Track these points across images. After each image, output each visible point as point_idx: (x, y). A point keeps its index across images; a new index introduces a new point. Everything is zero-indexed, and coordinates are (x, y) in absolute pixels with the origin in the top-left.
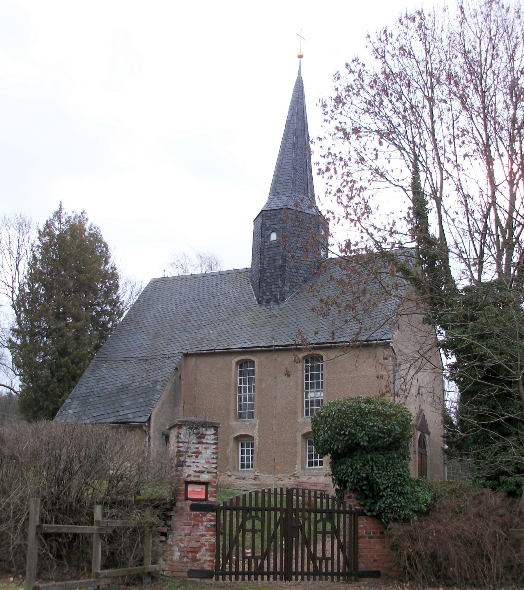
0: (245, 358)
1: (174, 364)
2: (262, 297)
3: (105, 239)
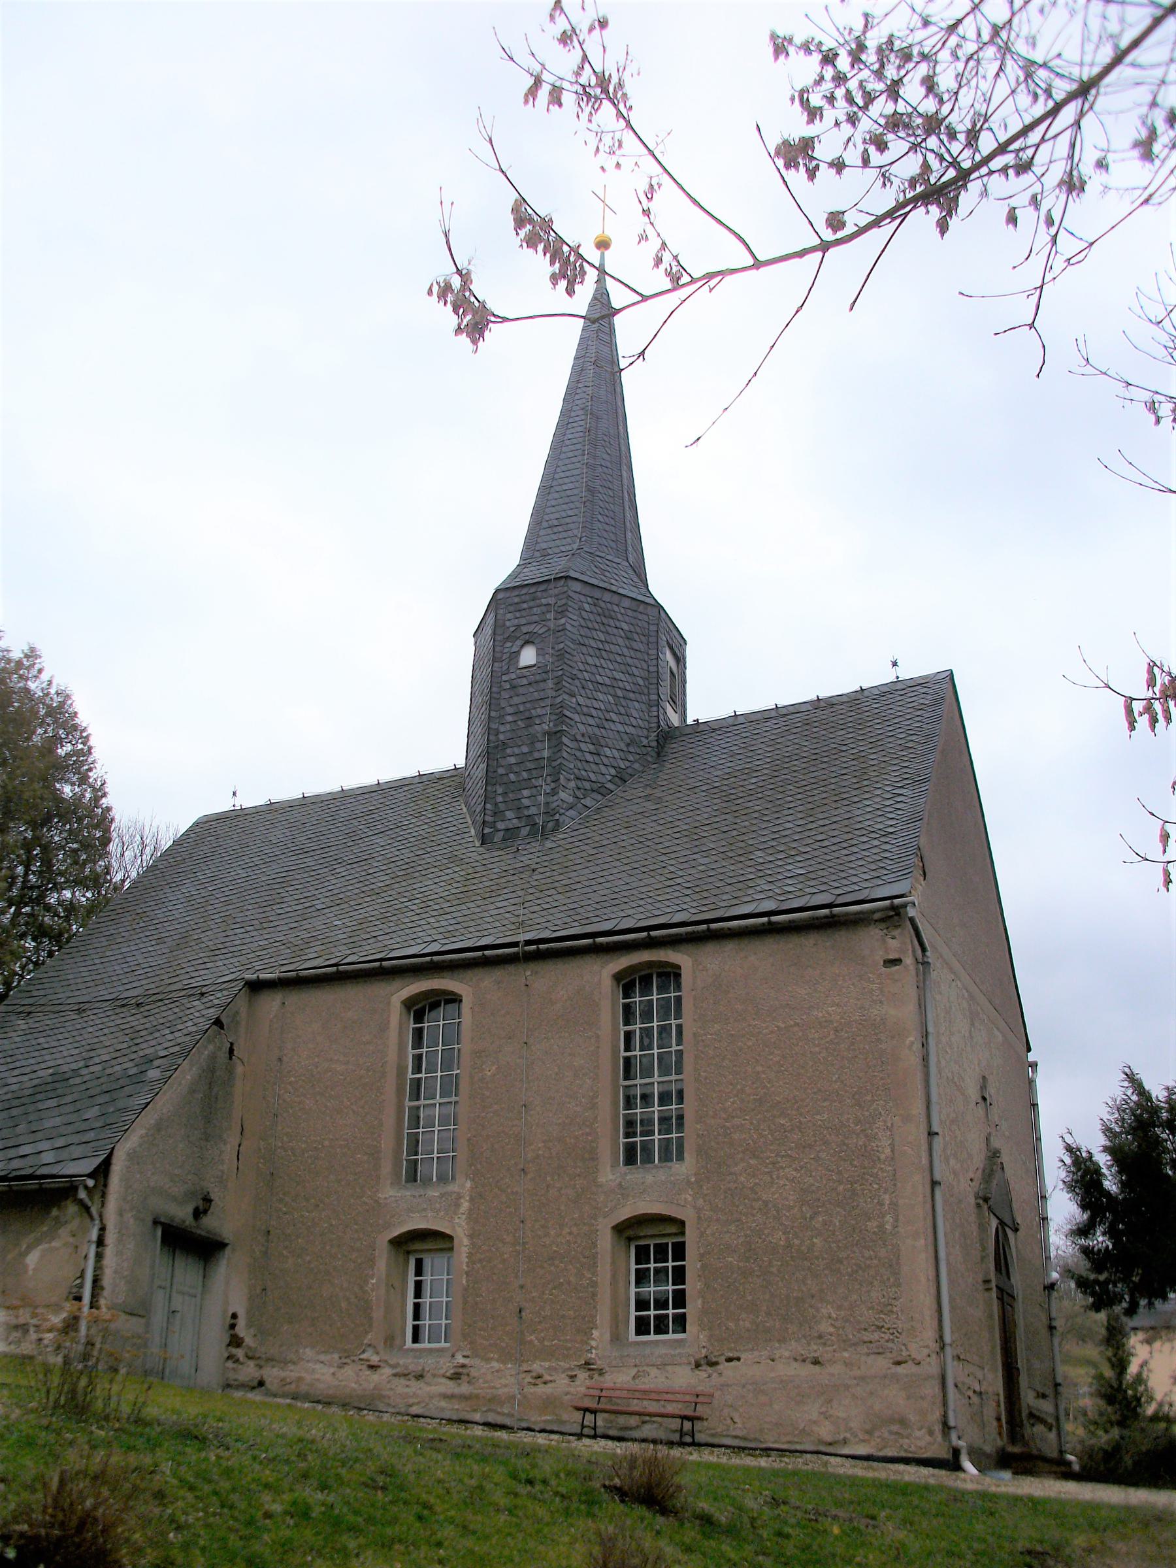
0: (429, 984)
1: (212, 1010)
2: (493, 825)
3: (83, 719)
